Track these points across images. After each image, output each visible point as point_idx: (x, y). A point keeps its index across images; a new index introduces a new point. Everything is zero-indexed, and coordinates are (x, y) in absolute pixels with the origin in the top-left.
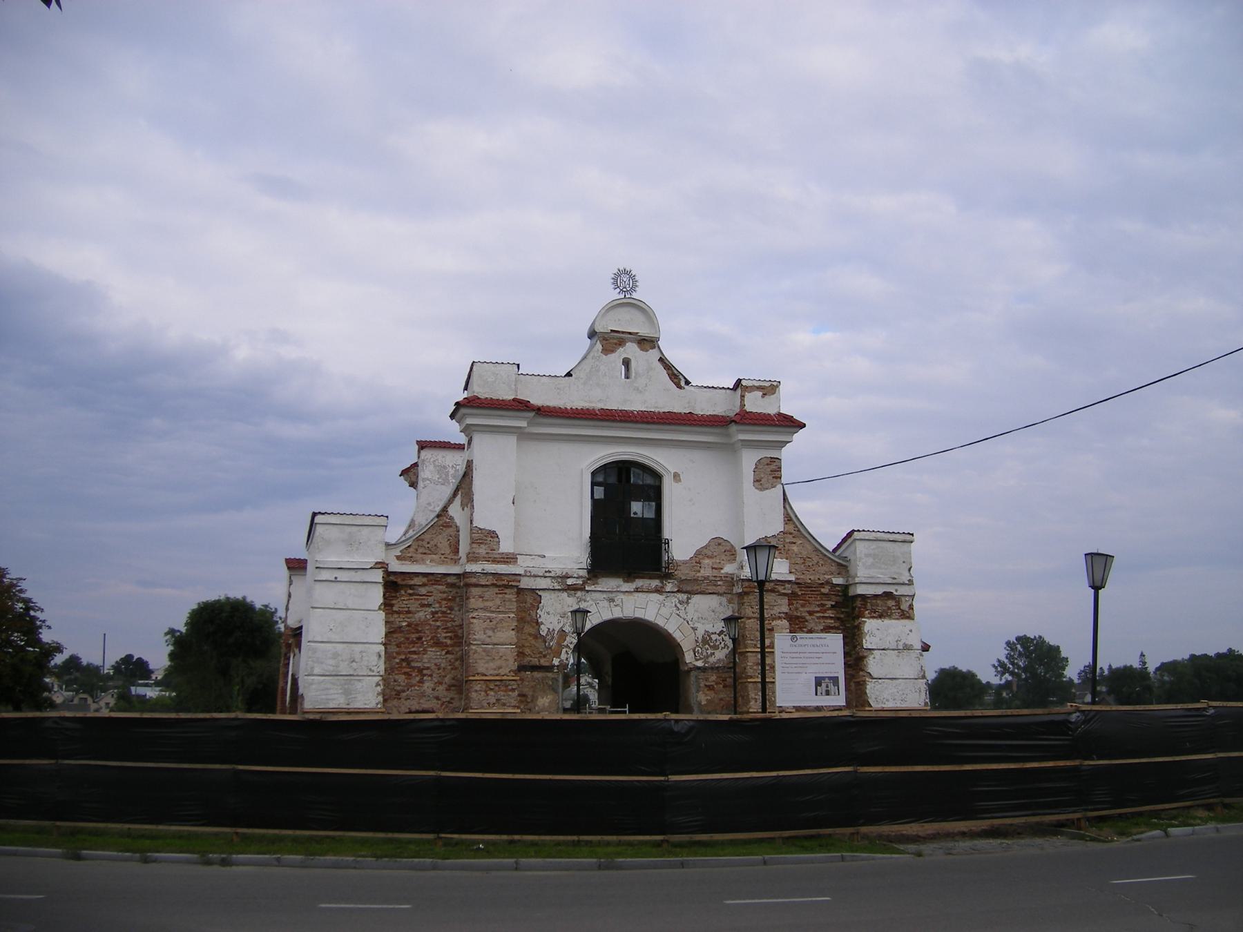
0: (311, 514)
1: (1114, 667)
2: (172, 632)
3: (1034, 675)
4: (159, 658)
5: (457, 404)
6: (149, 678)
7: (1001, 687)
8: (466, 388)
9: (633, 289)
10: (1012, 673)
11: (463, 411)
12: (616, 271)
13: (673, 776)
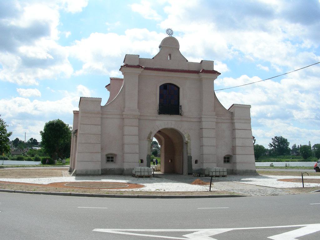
0: (80, 98)
1: (205, 171)
2: (41, 132)
3: (280, 147)
4: (39, 139)
5: (121, 66)
6: (37, 144)
7: (271, 150)
8: (124, 62)
9: (172, 34)
10: (273, 147)
11: (123, 68)
12: (167, 29)
13: (72, 181)
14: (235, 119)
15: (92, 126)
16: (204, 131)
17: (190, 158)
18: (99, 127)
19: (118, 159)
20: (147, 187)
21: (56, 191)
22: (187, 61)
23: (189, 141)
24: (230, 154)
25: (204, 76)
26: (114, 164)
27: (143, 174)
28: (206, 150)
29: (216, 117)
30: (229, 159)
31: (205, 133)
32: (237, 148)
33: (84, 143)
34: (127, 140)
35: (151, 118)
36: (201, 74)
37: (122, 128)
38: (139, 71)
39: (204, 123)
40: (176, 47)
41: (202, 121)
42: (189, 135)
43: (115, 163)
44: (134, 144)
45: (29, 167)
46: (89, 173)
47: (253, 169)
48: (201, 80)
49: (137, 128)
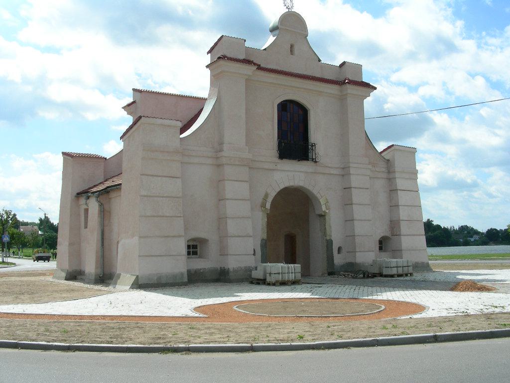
14: (397, 172)
15: (164, 178)
16: (354, 191)
17: (329, 243)
18: (179, 181)
19: (213, 249)
20: (190, 307)
21: (316, 337)
22: (320, 60)
23: (327, 211)
24: (388, 234)
25: (351, 89)
26: (199, 259)
27: (286, 277)
28: (360, 228)
29: (370, 167)
30: (193, 255)
31: (357, 197)
32: (402, 224)
33: (151, 216)
34: (231, 208)
35: (266, 166)
36: (348, 86)
37: (218, 183)
38: (249, 70)
39: (353, 178)
40: (303, 32)
41: (350, 174)
42: (327, 199)
43: (200, 257)
44: (243, 217)
45: (44, 274)
46: (163, 281)
47: (425, 260)
48: (342, 99)
49: (246, 186)
